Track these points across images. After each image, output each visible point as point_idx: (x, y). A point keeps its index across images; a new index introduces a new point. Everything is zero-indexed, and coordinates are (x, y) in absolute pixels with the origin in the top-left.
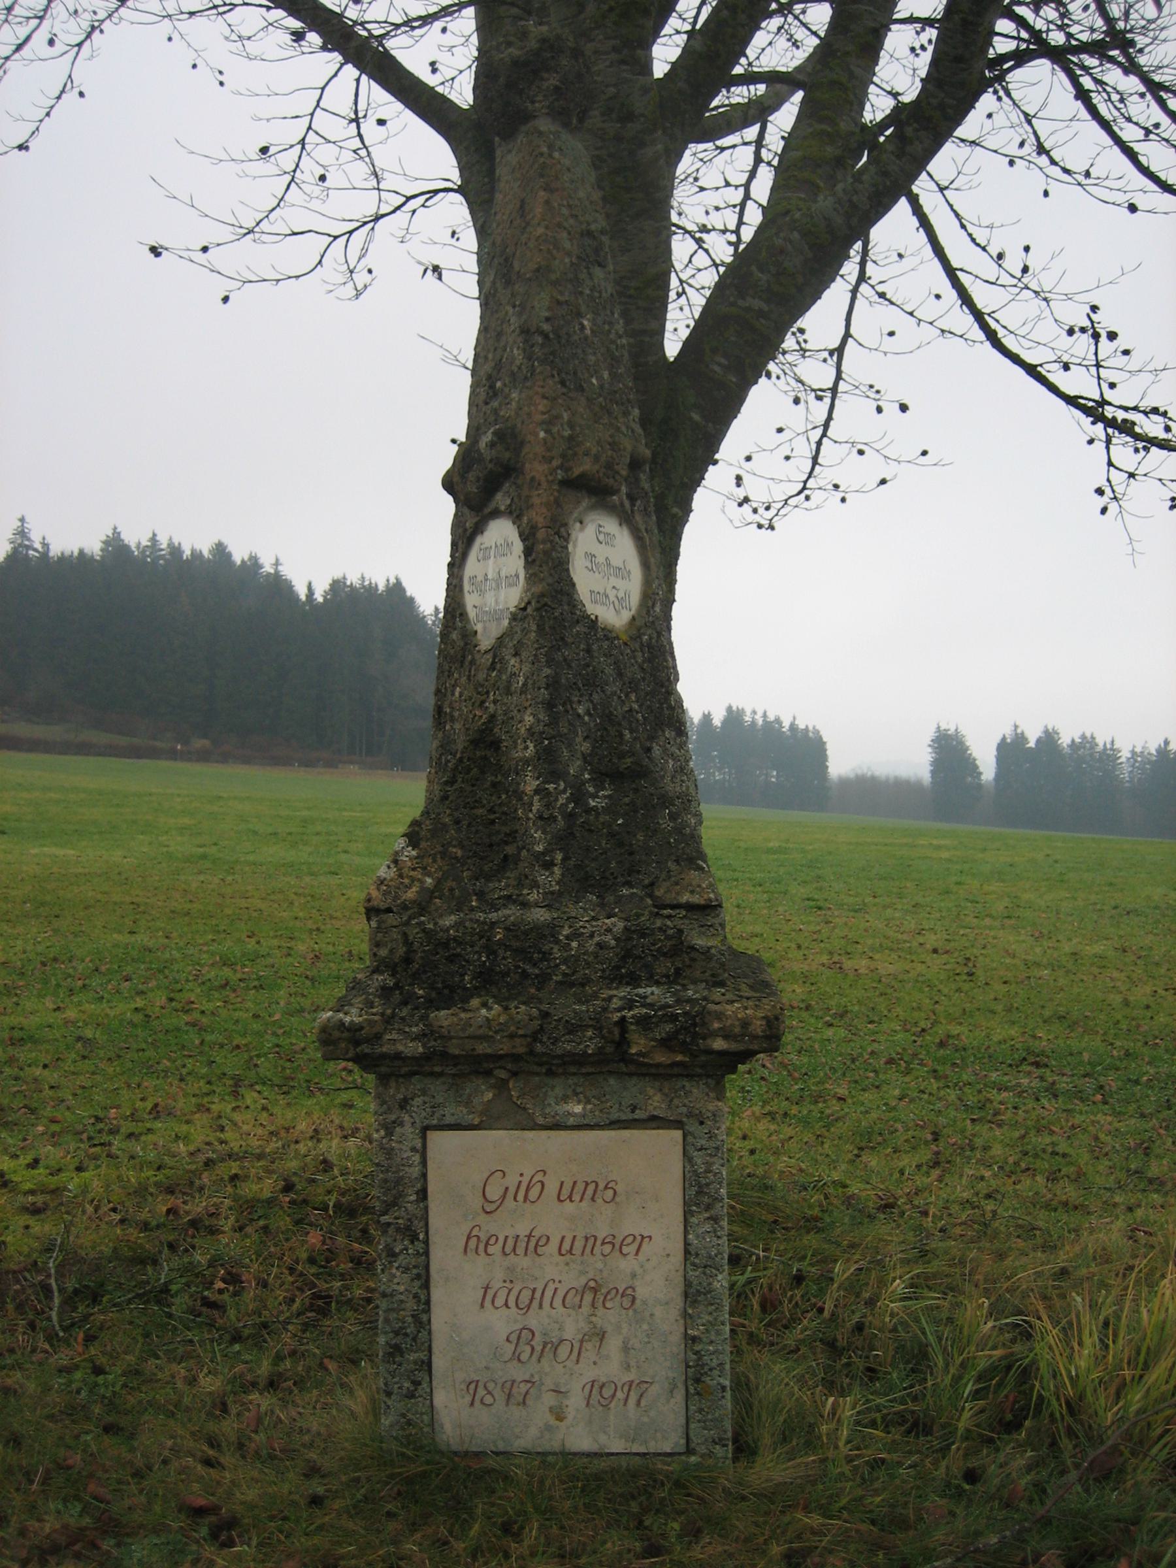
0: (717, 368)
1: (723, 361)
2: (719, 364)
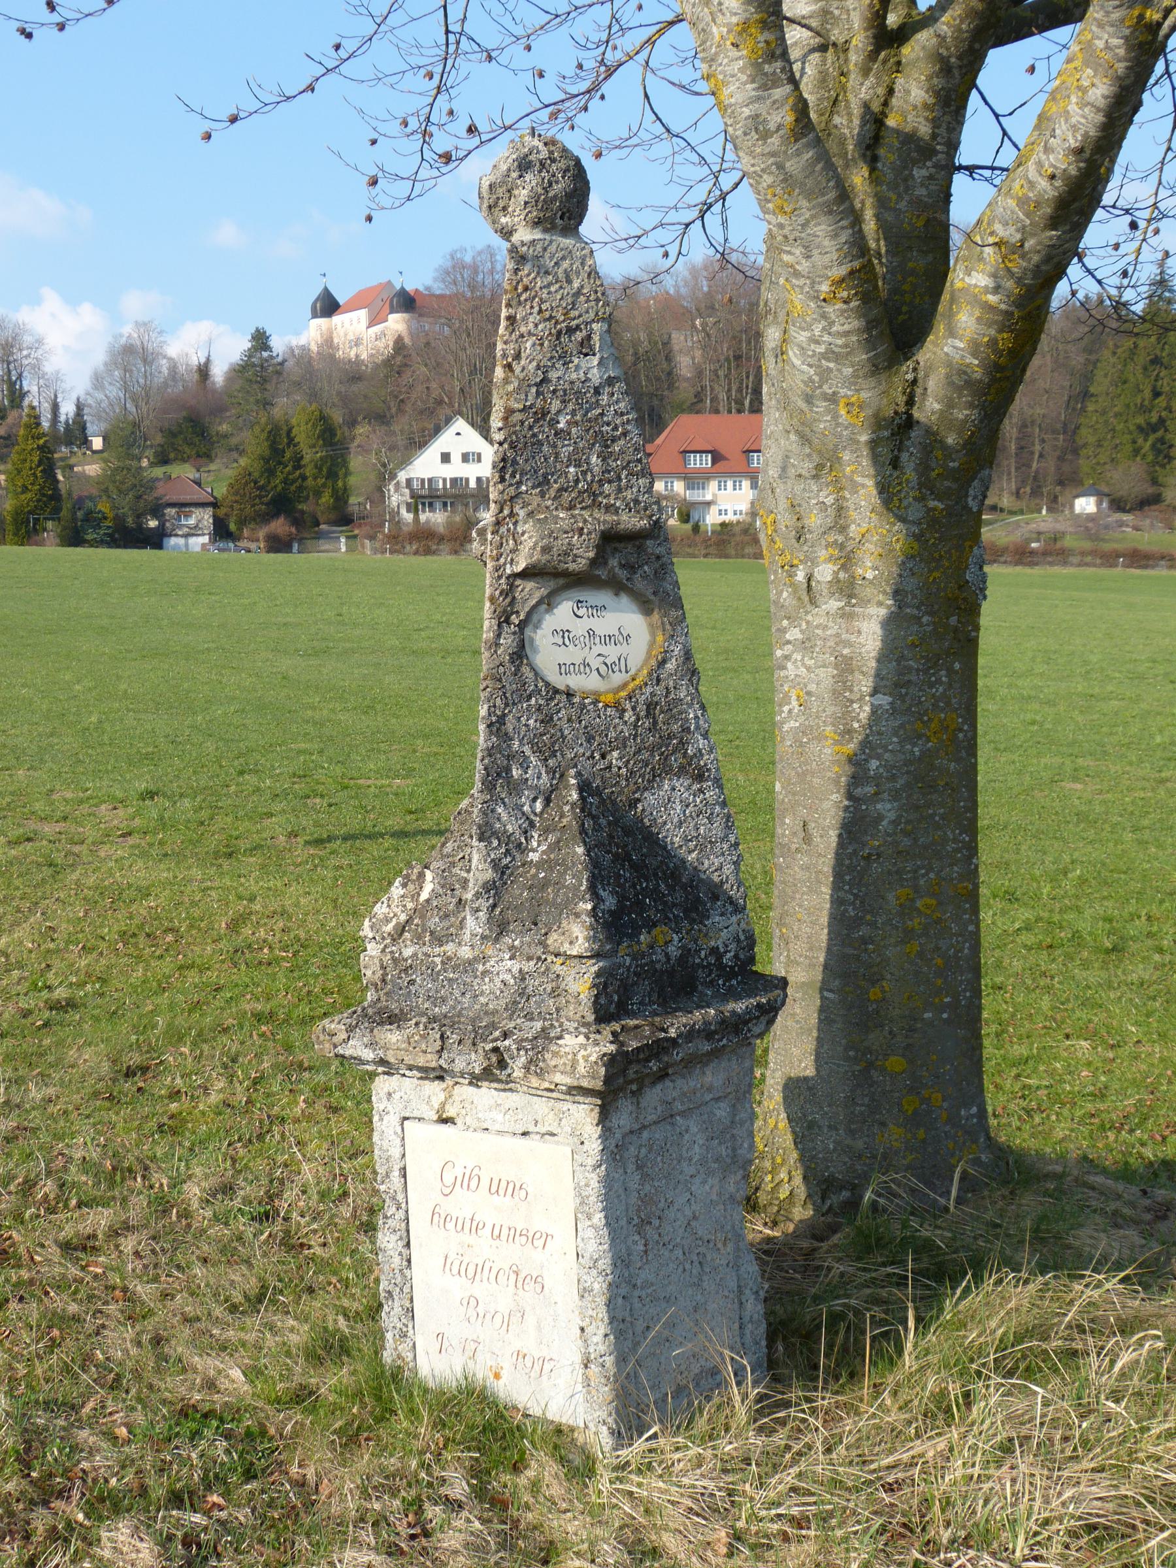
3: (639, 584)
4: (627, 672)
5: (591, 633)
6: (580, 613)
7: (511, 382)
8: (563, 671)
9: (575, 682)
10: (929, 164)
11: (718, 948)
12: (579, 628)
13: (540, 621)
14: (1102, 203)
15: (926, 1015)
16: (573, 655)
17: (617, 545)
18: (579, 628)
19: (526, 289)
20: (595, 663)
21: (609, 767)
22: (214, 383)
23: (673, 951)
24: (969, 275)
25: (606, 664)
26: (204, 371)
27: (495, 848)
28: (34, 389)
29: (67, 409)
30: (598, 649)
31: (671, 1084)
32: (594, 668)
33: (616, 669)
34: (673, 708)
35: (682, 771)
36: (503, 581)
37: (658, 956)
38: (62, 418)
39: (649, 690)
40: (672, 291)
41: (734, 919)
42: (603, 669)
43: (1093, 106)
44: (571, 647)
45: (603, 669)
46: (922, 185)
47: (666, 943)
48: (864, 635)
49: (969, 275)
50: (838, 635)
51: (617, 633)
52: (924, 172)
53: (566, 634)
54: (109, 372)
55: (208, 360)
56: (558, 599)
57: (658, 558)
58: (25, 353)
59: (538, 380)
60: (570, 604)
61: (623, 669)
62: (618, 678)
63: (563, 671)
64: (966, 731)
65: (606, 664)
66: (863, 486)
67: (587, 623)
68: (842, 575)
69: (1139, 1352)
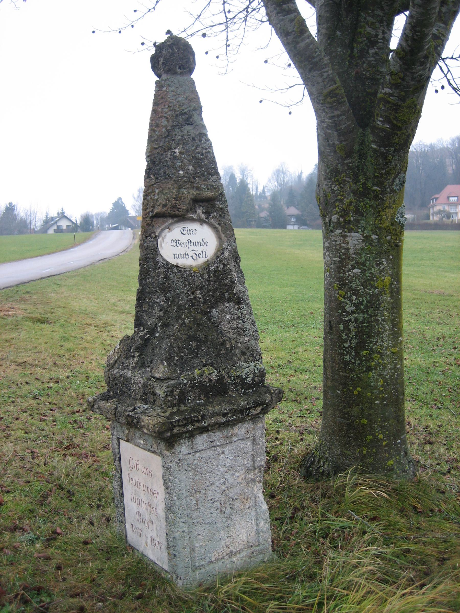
0: (379, 123)
1: (381, 119)
2: (380, 121)
3: (211, 220)
4: (206, 257)
5: (189, 241)
6: (184, 233)
7: (154, 137)
8: (176, 257)
9: (181, 262)
10: (375, 47)
11: (242, 376)
12: (184, 239)
13: (165, 236)
14: (443, 56)
15: (376, 402)
16: (180, 250)
17: (201, 204)
18: (184, 239)
19: (162, 98)
20: (191, 254)
21: (195, 298)
22: (303, 179)
23: (214, 377)
24: (383, 89)
25: (196, 254)
26: (300, 176)
27: (142, 331)
28: (251, 182)
29: (260, 189)
30: (193, 248)
31: (213, 434)
32: (190, 255)
33: (201, 256)
34: (226, 272)
35: (229, 300)
36: (148, 219)
37: (205, 379)
38: (259, 191)
39: (216, 265)
40: (445, 146)
41: (253, 364)
42: (194, 256)
43: (417, 5)
44: (180, 247)
45: (194, 256)
46: (373, 56)
47: (210, 374)
48: (349, 244)
49: (383, 89)
50: (340, 244)
51: (201, 241)
52: (373, 51)
53: (178, 241)
54: (273, 177)
55: (301, 173)
56: (174, 227)
57: (221, 209)
58: (249, 172)
59: (166, 135)
60: (180, 229)
61: (204, 256)
62: (201, 261)
63: (176, 257)
64: (395, 284)
65: (196, 254)
66: (348, 182)
67: (187, 237)
68: (341, 219)
69: (328, 608)
